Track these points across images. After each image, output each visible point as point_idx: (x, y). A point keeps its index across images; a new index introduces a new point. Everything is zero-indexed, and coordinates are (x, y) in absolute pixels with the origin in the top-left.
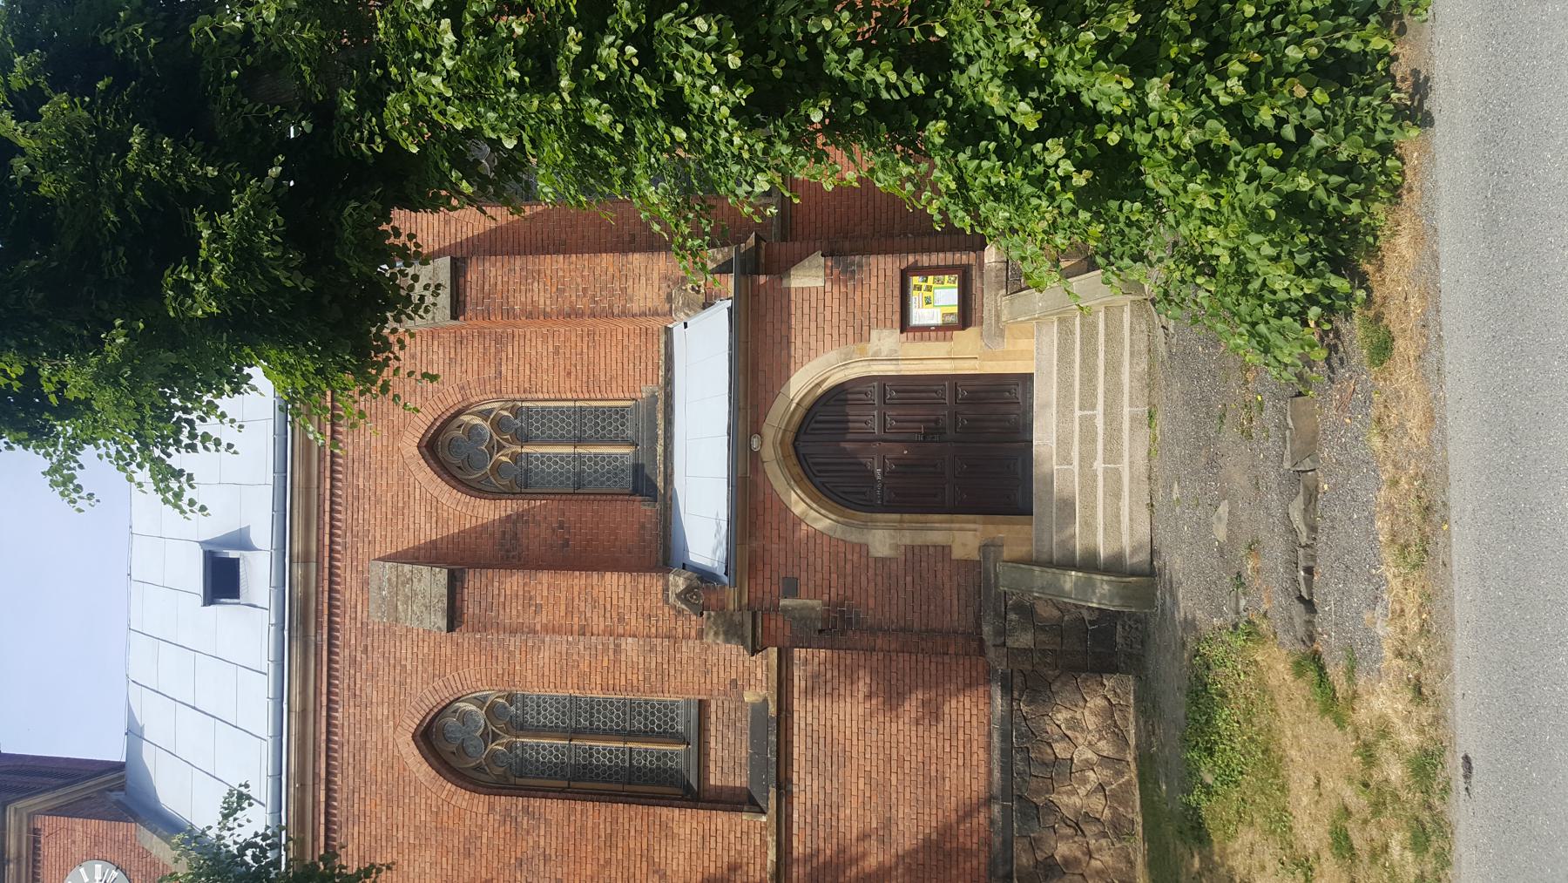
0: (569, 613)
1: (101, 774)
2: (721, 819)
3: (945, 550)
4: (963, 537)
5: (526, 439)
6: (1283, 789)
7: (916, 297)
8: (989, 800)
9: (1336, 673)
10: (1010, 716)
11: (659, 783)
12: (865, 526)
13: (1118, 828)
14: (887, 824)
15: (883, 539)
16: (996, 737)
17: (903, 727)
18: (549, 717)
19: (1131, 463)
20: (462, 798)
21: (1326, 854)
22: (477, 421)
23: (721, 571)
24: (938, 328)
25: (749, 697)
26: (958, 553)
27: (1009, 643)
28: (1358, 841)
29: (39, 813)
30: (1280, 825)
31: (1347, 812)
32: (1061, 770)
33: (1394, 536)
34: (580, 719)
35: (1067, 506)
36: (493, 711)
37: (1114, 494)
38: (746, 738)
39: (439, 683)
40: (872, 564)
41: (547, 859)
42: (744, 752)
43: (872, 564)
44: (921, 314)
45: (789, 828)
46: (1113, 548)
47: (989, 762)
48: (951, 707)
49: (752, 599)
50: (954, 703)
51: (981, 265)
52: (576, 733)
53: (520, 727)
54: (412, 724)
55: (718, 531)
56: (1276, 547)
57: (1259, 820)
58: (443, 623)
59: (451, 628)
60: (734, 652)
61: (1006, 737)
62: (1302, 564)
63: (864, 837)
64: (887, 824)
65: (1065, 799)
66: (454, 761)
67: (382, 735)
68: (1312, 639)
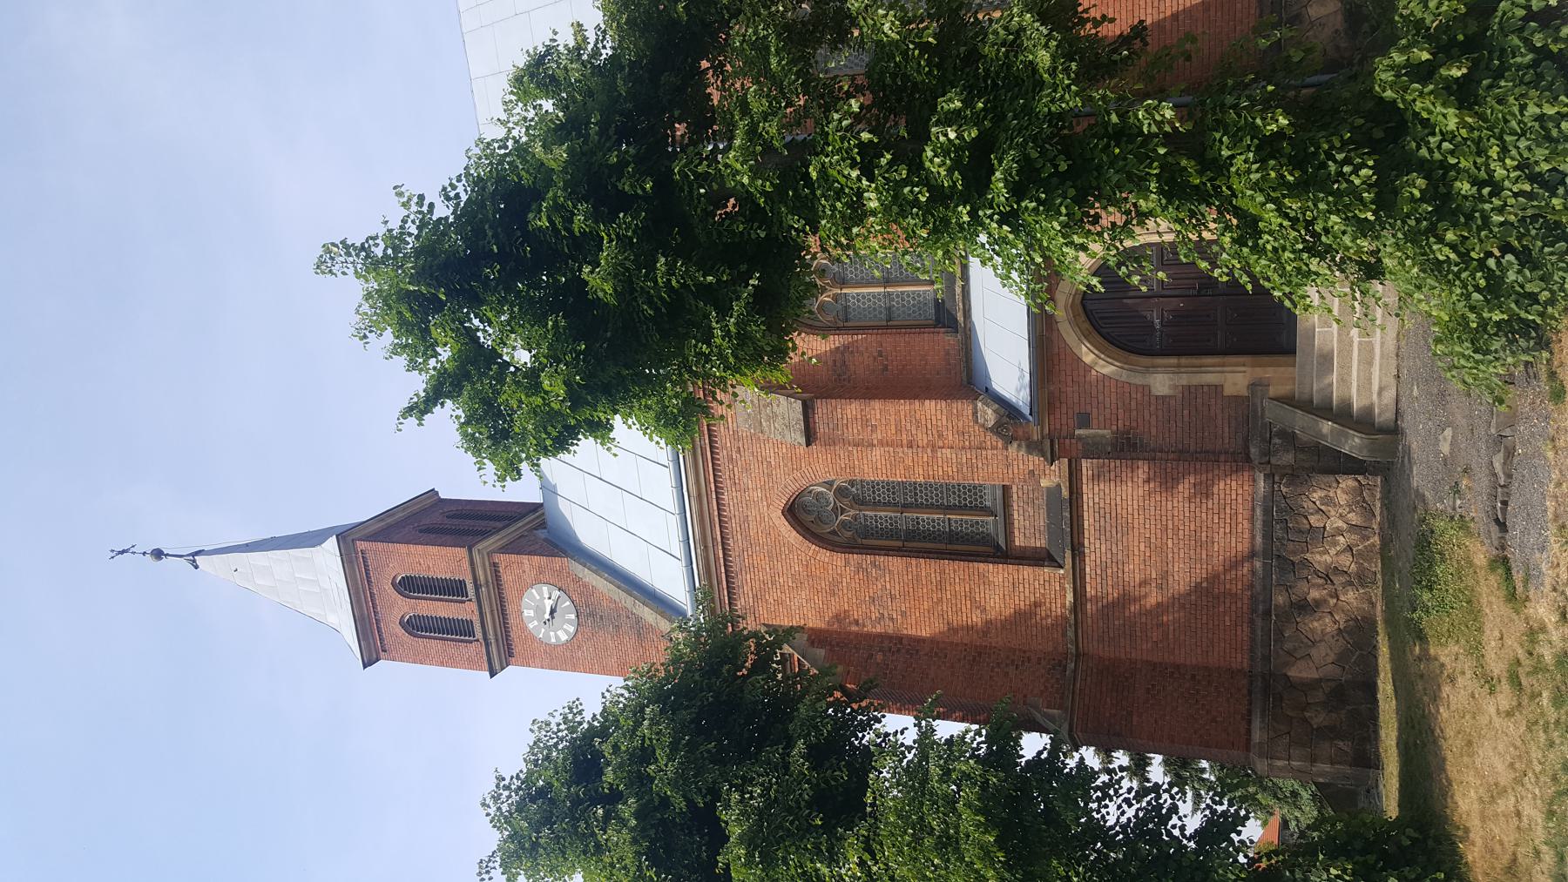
0: (899, 430)
1: (523, 516)
2: (1027, 572)
3: (1217, 389)
4: (1235, 377)
5: (843, 283)
6: (1480, 630)
8: (1252, 554)
9: (1518, 577)
10: (1271, 496)
11: (973, 543)
12: (1148, 369)
13: (1361, 579)
14: (1165, 575)
15: (1162, 381)
16: (1258, 511)
17: (1179, 503)
18: (884, 496)
19: (1382, 344)
20: (824, 555)
21: (1504, 681)
22: (821, 489)
23: (1026, 411)
25: (1044, 483)
26: (1228, 391)
27: (1273, 461)
28: (1524, 682)
29: (494, 552)
30: (1476, 651)
31: (1518, 662)
32: (1317, 536)
33: (1556, 517)
34: (908, 496)
35: (1326, 360)
37: (1367, 362)
38: (1043, 512)
39: (797, 474)
40: (1153, 401)
41: (893, 598)
42: (1042, 521)
43: (1153, 401)
45: (1083, 578)
46: (1365, 402)
47: (1252, 531)
48: (1220, 487)
49: (1053, 417)
50: (1222, 485)
52: (906, 507)
53: (860, 502)
55: (1021, 377)
56: (1484, 482)
57: (1463, 642)
58: (803, 440)
59: (808, 444)
60: (1035, 461)
61: (1267, 511)
62: (1500, 498)
63: (1143, 583)
64: (1165, 575)
65: (1318, 557)
66: (813, 528)
67: (759, 511)
68: (1503, 548)
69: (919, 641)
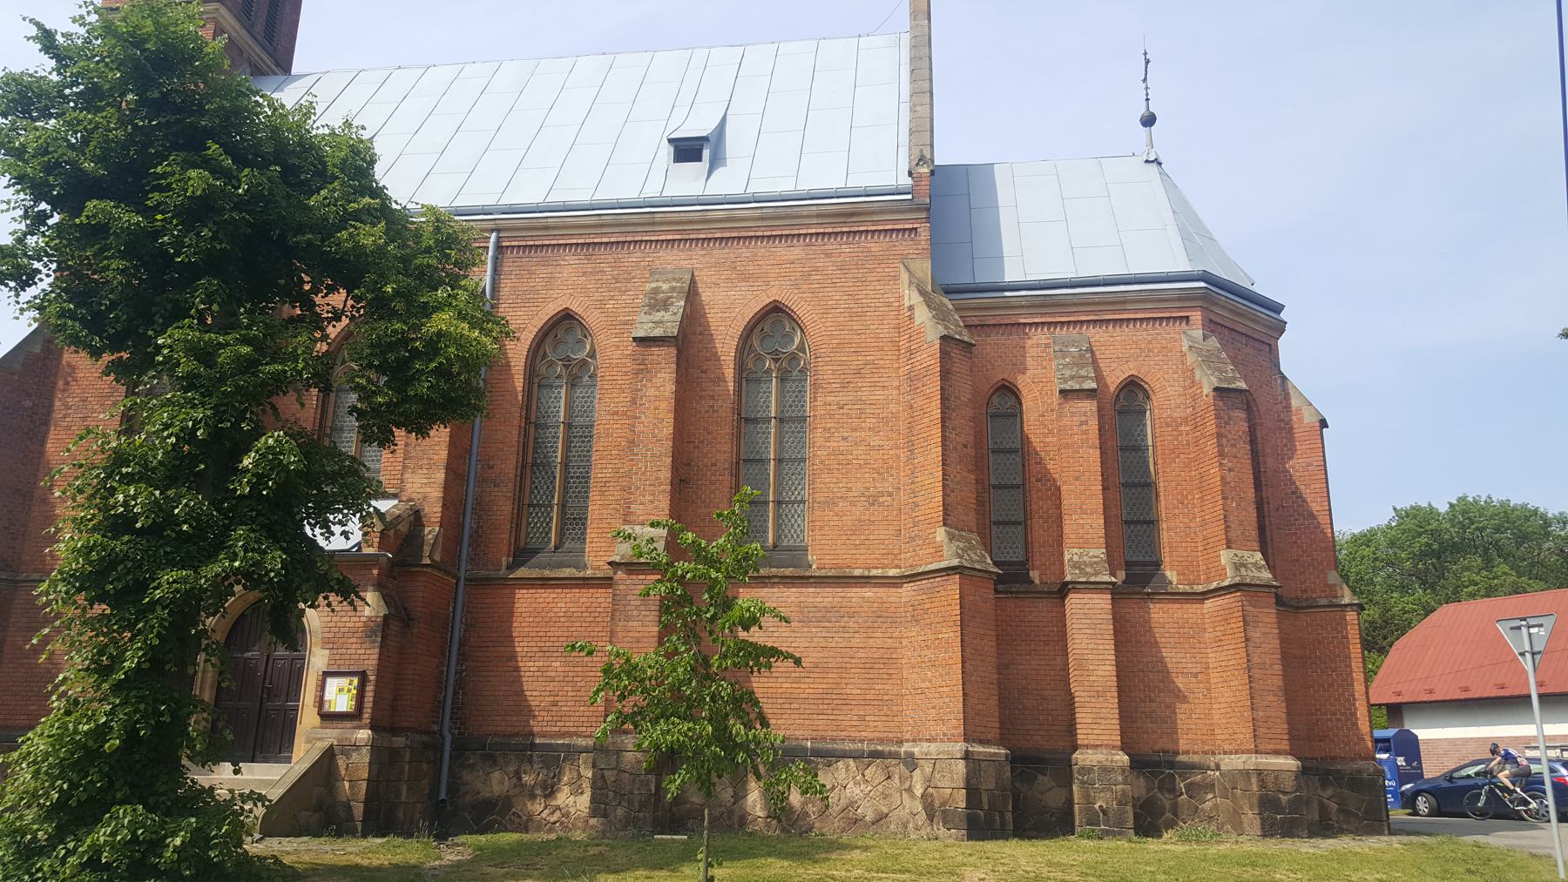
5: (782, 380)
7: (343, 682)
22: (797, 341)
24: (322, 697)
36: (793, 358)
41: (84, 418)
44: (333, 684)
51: (360, 728)
53: (573, 383)
54: (575, 307)
66: (551, 336)
69: (43, 442)
